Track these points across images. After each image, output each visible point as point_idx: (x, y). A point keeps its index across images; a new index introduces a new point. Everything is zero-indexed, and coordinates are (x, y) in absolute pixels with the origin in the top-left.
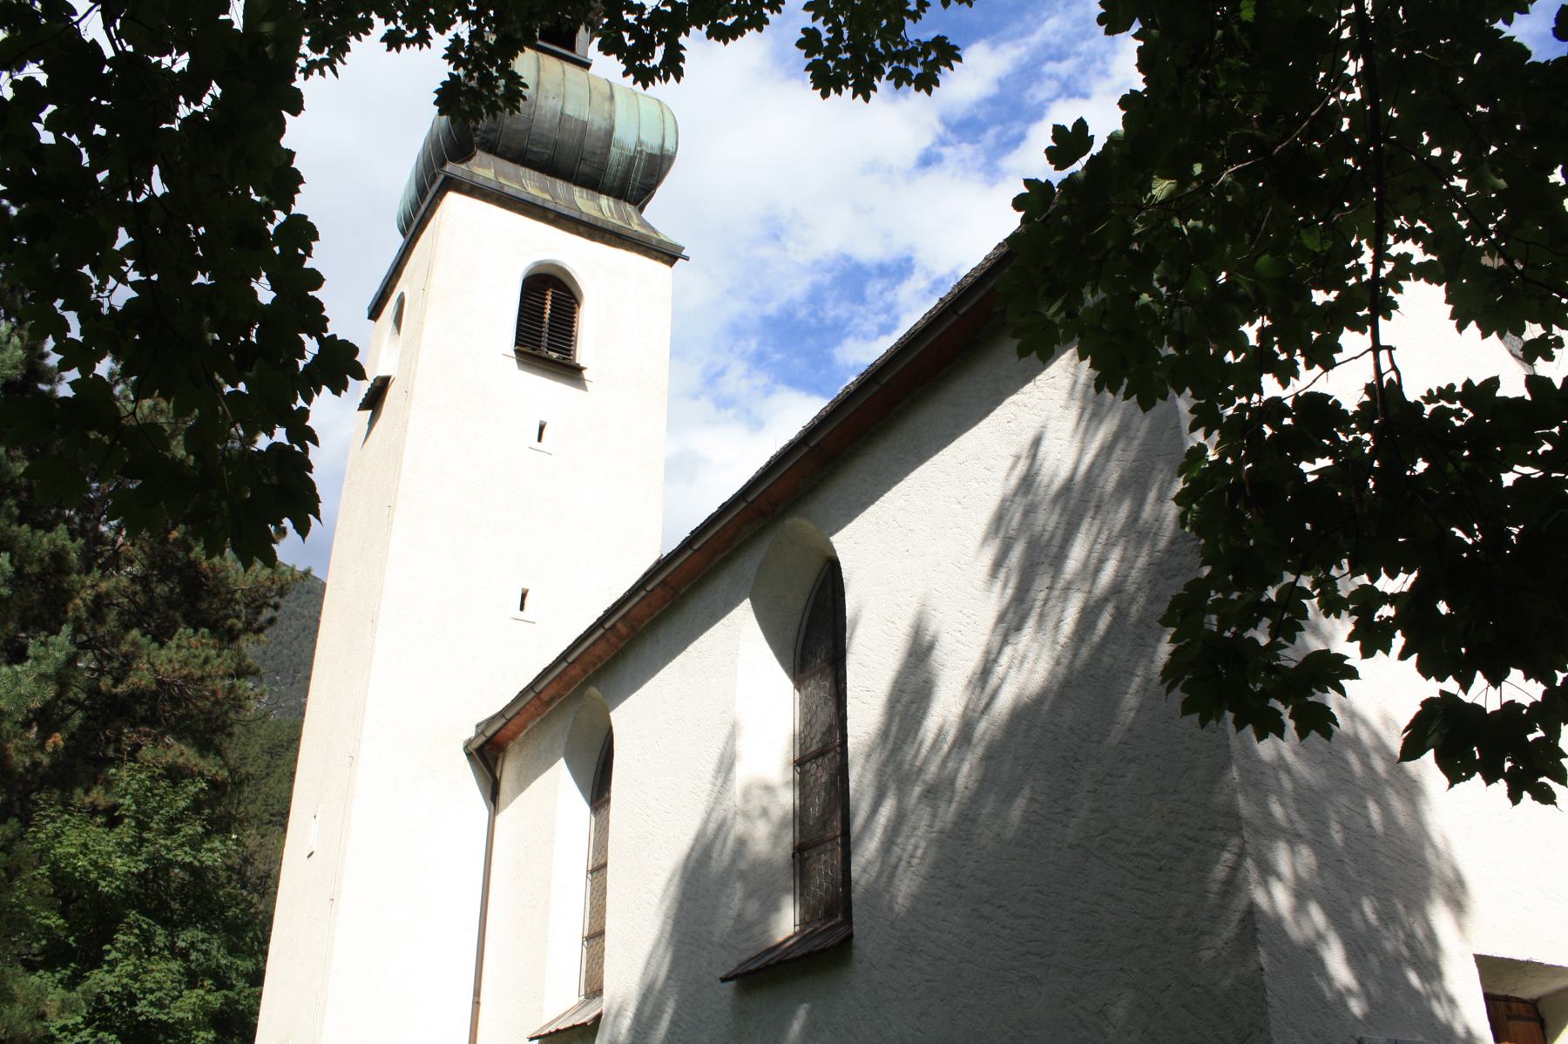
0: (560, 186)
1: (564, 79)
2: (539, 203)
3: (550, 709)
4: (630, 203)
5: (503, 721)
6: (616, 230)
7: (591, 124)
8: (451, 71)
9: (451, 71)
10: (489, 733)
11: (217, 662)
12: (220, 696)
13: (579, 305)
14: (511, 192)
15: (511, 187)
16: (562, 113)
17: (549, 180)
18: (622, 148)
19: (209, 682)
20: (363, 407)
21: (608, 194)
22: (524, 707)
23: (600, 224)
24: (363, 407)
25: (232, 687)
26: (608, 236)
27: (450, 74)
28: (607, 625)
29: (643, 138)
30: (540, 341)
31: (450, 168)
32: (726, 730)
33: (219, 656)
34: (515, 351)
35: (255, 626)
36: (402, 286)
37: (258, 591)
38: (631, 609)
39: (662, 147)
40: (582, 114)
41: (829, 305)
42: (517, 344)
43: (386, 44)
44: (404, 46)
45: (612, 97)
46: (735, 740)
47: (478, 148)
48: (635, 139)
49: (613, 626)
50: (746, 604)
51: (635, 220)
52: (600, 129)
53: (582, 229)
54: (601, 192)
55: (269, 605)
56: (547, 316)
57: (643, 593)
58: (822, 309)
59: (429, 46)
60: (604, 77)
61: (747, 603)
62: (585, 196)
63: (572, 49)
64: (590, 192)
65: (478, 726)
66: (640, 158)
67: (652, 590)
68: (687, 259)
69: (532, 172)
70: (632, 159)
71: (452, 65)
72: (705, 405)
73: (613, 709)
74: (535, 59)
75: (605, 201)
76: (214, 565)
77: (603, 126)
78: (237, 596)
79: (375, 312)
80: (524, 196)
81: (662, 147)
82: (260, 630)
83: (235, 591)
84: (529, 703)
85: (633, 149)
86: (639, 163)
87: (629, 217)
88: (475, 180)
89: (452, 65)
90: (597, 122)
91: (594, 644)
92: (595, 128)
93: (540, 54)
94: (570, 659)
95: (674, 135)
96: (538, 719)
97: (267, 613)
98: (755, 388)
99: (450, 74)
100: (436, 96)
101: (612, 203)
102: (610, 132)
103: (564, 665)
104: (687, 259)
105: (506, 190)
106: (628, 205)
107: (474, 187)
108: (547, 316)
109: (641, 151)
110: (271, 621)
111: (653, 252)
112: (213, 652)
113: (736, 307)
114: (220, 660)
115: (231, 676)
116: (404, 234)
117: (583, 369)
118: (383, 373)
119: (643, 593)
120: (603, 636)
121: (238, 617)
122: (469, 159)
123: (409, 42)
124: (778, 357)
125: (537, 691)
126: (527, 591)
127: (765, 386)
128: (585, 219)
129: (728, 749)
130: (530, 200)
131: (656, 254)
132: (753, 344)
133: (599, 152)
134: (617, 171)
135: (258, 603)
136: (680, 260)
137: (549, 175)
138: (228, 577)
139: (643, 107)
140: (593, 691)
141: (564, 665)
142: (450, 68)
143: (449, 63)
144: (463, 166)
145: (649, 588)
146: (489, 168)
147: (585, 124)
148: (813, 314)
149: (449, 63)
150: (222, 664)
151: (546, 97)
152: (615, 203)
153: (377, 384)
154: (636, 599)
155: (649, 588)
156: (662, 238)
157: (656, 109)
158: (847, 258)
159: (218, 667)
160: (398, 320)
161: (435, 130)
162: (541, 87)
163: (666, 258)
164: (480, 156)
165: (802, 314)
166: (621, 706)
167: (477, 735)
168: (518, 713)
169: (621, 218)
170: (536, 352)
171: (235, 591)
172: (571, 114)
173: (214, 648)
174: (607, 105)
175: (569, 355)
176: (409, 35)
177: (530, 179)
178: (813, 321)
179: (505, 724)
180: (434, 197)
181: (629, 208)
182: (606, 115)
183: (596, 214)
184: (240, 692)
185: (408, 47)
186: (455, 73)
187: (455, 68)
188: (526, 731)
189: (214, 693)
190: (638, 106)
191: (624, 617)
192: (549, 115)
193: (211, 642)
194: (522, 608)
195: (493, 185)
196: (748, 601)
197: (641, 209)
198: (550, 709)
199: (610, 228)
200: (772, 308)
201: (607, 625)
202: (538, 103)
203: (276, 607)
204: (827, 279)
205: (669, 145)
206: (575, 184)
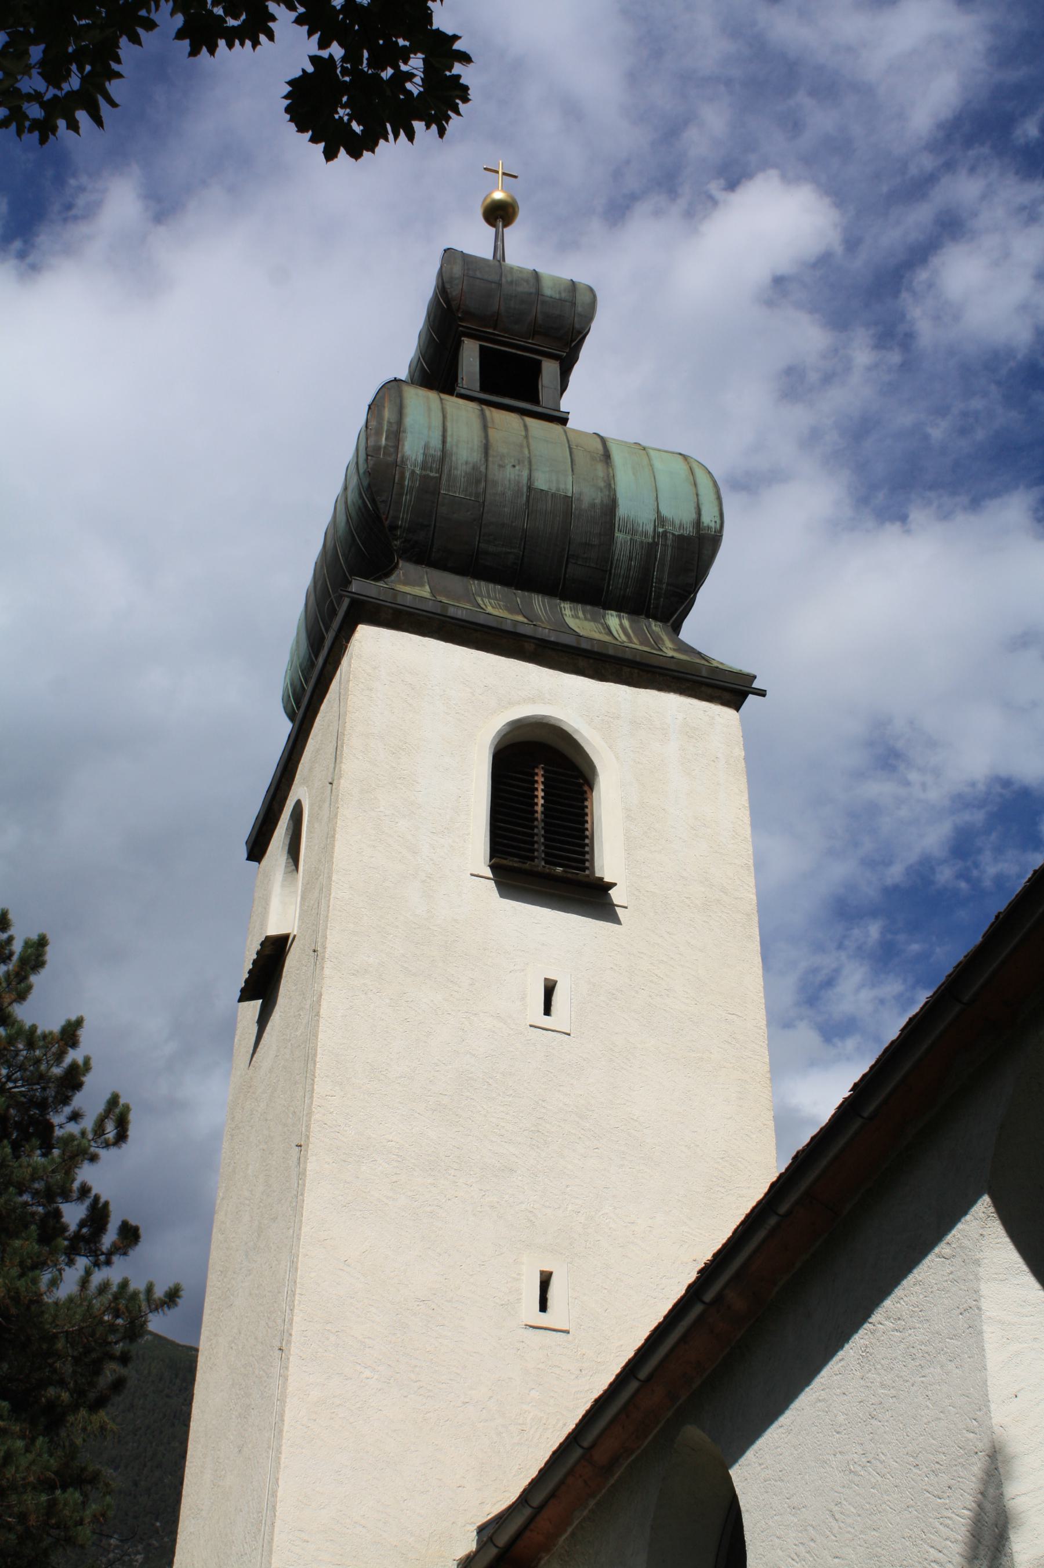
0: (539, 603)
1: (526, 437)
2: (509, 627)
3: (612, 1481)
4: (656, 619)
5: (527, 1512)
6: (638, 659)
7: (579, 500)
8: (315, 51)
9: (315, 51)
10: (503, 1540)
11: (24, 1461)
12: (33, 1520)
13: (592, 789)
14: (460, 614)
15: (460, 609)
16: (535, 324)
17: (519, 597)
18: (633, 532)
19: (13, 1499)
20: (246, 995)
21: (619, 607)
22: (562, 1482)
23: (611, 652)
24: (246, 995)
25: (52, 1504)
26: (626, 670)
27: (314, 59)
28: (708, 1297)
29: (665, 512)
30: (533, 851)
31: (358, 586)
32: (977, 1466)
33: (27, 1450)
34: (492, 867)
35: (92, 1395)
36: (299, 791)
37: (93, 1334)
38: (750, 1258)
39: (698, 523)
40: (562, 486)
41: (986, 857)
42: (492, 856)
43: (187, 42)
44: (222, 43)
45: (607, 456)
46: (1000, 1485)
47: (400, 557)
48: (653, 516)
49: (719, 1298)
50: (984, 1205)
51: (668, 644)
52: (593, 506)
53: (582, 663)
54: (607, 606)
55: (112, 1357)
56: (539, 808)
57: (773, 1221)
58: (976, 865)
59: (271, 36)
60: (592, 432)
61: (984, 1205)
62: (581, 614)
63: (536, 401)
64: (589, 607)
65: (481, 1530)
66: (665, 545)
67: (789, 1213)
68: (762, 693)
69: (491, 586)
70: (652, 547)
71: (316, 37)
72: (806, 1036)
73: (735, 1460)
74: (477, 412)
75: (613, 620)
76: (17, 1292)
77: (598, 501)
78: (60, 1345)
79: (257, 849)
80: (481, 620)
81: (698, 523)
82: (99, 1403)
83: (55, 1336)
84: (571, 1472)
85: (650, 529)
86: (664, 554)
87: (657, 640)
88: (399, 601)
89: (316, 37)
90: (589, 494)
91: (684, 1339)
92: (585, 505)
93: (484, 407)
94: (643, 1374)
95: (716, 503)
96: (592, 1503)
97: (111, 1371)
98: (882, 1002)
99: (314, 59)
100: (288, 88)
101: (626, 623)
102: (611, 506)
103: (634, 1385)
104: (762, 693)
105: (451, 612)
106: (653, 623)
107: (400, 612)
108: (539, 808)
109: (665, 533)
110: (118, 1385)
111: (703, 689)
112: (20, 1444)
113: (840, 871)
114: (30, 1457)
115: (51, 1487)
116: (292, 716)
117: (612, 885)
118: (274, 930)
119: (773, 1221)
120: (700, 1319)
121: (62, 1383)
122: (388, 574)
123: (233, 37)
124: (915, 947)
125: (586, 1444)
126: (550, 1274)
127: (898, 997)
128: (584, 645)
129: (988, 1506)
130: (494, 624)
131: (709, 691)
132: (874, 930)
133: (596, 541)
134: (629, 569)
135: (94, 1355)
136: (751, 698)
137: (522, 588)
138: (43, 1312)
139: (658, 464)
140: (692, 1432)
141: (634, 1385)
142: (312, 46)
143: (310, 34)
144: (381, 584)
145: (783, 1209)
146: (422, 585)
147: (568, 500)
148: (963, 875)
149: (310, 34)
150: (33, 1462)
151: (501, 466)
152: (631, 621)
153: (267, 952)
154: (761, 1234)
155: (783, 1209)
156: (715, 664)
157: (681, 466)
158: (1006, 783)
159: (28, 1468)
160: (294, 851)
161: (330, 544)
162: (491, 452)
163: (727, 696)
164: (405, 568)
165: (945, 875)
166: (750, 1454)
167: (482, 1545)
168: (552, 1495)
169: (644, 641)
170: (527, 866)
171: (55, 1336)
172: (544, 487)
173: (23, 1437)
174: (600, 470)
175: (584, 869)
176: (231, 22)
177: (489, 597)
178: (963, 885)
179: (531, 1519)
180: (336, 638)
181: (656, 627)
182: (602, 484)
183: (607, 638)
184: (67, 1512)
185: (230, 45)
186: (324, 54)
187: (323, 44)
188: (570, 1530)
189: (23, 1517)
190: (651, 465)
191: (737, 1276)
192: (509, 493)
193: (16, 1428)
194: (543, 1307)
195: (430, 607)
196: (986, 1199)
197: (677, 628)
198: (612, 1481)
199: (628, 656)
200: (895, 873)
201: (708, 1297)
202: (490, 477)
203: (124, 1359)
204: (978, 817)
205: (708, 518)
206: (564, 598)
